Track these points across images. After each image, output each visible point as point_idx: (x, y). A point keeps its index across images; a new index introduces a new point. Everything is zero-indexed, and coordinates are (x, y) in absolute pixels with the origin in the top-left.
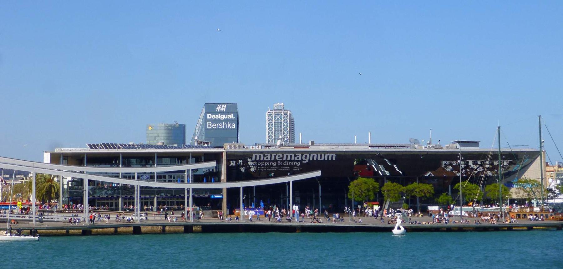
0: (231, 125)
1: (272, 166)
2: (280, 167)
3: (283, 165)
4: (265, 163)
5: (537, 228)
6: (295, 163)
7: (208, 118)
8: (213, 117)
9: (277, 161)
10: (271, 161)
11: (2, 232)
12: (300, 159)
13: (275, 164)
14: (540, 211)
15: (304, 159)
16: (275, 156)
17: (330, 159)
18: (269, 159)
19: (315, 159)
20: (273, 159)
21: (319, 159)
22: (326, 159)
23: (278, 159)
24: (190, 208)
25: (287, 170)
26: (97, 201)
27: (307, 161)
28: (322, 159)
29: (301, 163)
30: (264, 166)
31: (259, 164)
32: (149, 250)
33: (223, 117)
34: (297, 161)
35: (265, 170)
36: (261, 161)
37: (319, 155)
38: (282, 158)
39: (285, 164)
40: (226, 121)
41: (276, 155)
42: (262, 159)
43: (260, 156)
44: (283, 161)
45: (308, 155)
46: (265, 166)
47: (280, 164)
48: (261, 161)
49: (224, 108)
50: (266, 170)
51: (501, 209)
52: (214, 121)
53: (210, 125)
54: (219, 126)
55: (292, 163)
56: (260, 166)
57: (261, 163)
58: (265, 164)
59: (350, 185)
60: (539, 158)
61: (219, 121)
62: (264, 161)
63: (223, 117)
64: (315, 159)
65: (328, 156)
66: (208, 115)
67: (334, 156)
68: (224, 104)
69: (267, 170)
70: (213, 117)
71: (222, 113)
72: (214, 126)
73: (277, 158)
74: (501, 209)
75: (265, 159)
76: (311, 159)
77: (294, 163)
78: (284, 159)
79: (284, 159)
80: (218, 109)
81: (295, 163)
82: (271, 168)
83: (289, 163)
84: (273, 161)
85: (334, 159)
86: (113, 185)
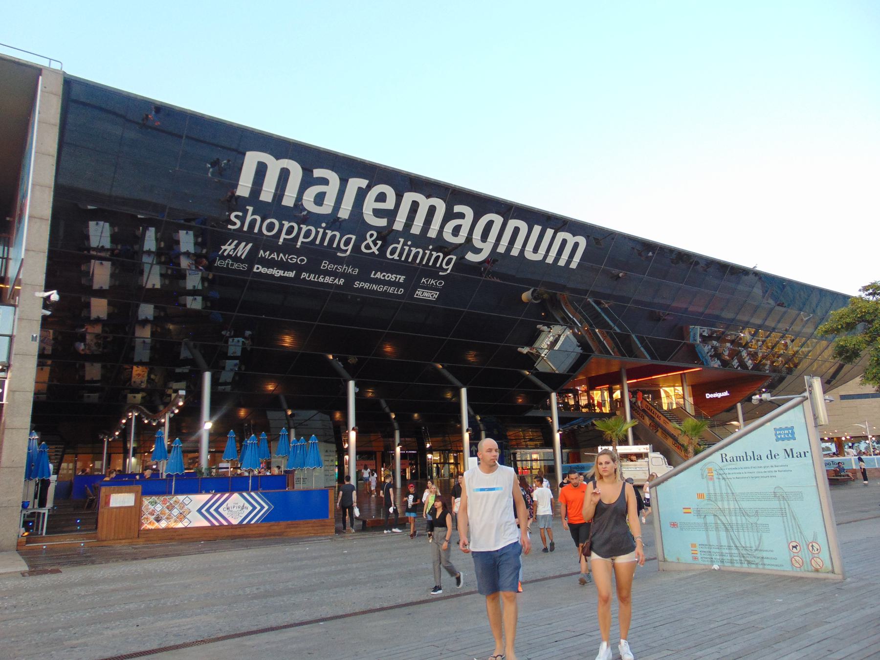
1: (330, 253)
4: (287, 225)
5: (347, 514)
6: (333, 238)
10: (333, 221)
11: (879, 650)
12: (461, 239)
13: (347, 243)
14: (137, 464)
18: (326, 209)
20: (344, 213)
21: (529, 255)
23: (370, 219)
24: (42, 511)
25: (391, 290)
28: (538, 257)
29: (461, 259)
30: (289, 247)
31: (271, 227)
35: (292, 274)
36: (283, 213)
38: (391, 215)
39: (397, 251)
41: (369, 187)
43: (284, 175)
46: (298, 253)
47: (371, 245)
48: (283, 213)
50: (298, 275)
55: (424, 254)
56: (271, 244)
57: (300, 229)
58: (306, 233)
59: (138, 367)
62: (298, 214)
69: (304, 275)
76: (501, 249)
77: (325, 234)
78: (398, 226)
79: (399, 225)
81: (333, 238)
82: (325, 265)
83: (435, 254)
86: (192, 343)
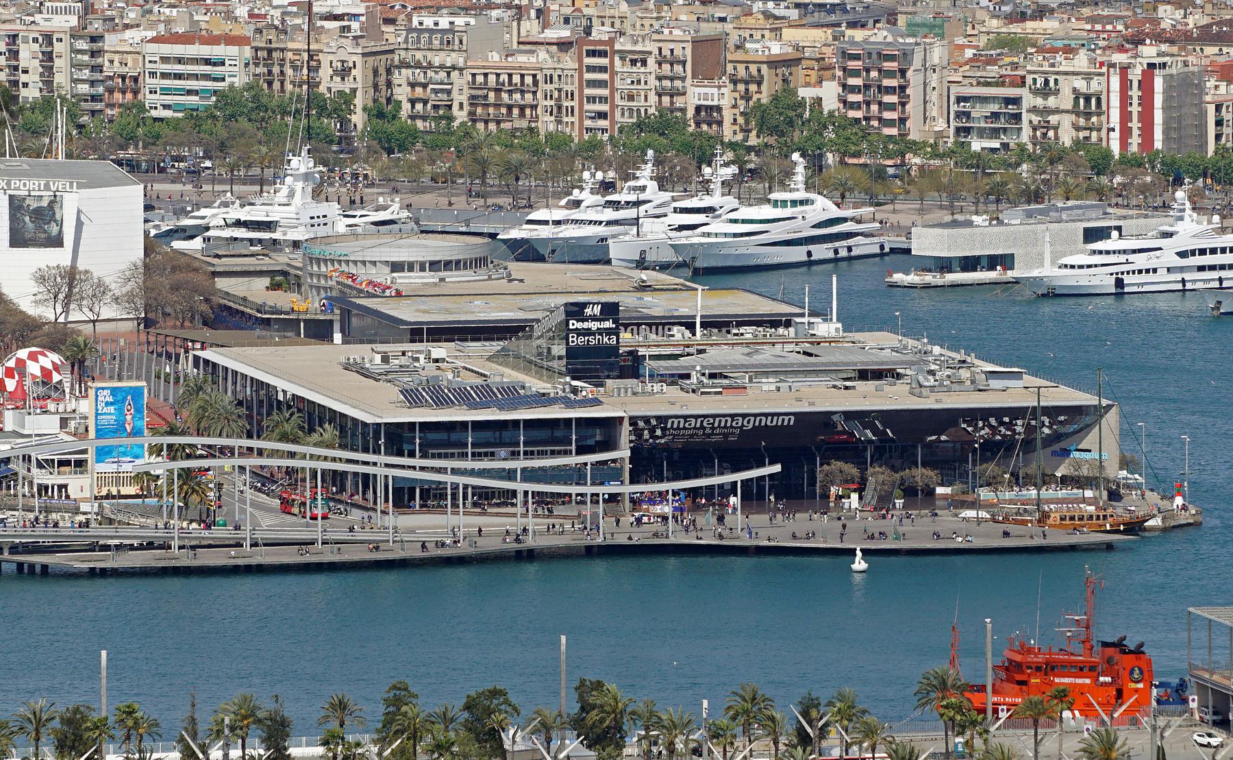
0: (609, 339)
1: (696, 434)
2: (709, 436)
3: (713, 434)
7: (571, 327)
8: (579, 325)
9: (704, 428)
10: (695, 428)
15: (745, 423)
16: (702, 422)
17: (786, 423)
18: (693, 425)
19: (763, 424)
21: (769, 423)
22: (780, 423)
26: (432, 492)
27: (751, 426)
28: (774, 423)
30: (684, 435)
32: (138, 478)
33: (594, 326)
34: (735, 428)
37: (770, 418)
38: (713, 424)
40: (600, 332)
42: (681, 426)
44: (713, 428)
45: (752, 419)
47: (708, 431)
49: (597, 310)
51: (1039, 494)
52: (579, 333)
53: (575, 340)
54: (588, 340)
60: (1098, 427)
61: (588, 332)
62: (685, 428)
63: (594, 326)
64: (763, 424)
65: (783, 420)
66: (571, 322)
67: (793, 418)
68: (598, 304)
70: (579, 325)
71: (594, 318)
72: (581, 341)
73: (705, 424)
74: (1039, 494)
75: (687, 425)
76: (757, 424)
78: (716, 425)
80: (588, 311)
84: (698, 429)
85: (792, 423)
